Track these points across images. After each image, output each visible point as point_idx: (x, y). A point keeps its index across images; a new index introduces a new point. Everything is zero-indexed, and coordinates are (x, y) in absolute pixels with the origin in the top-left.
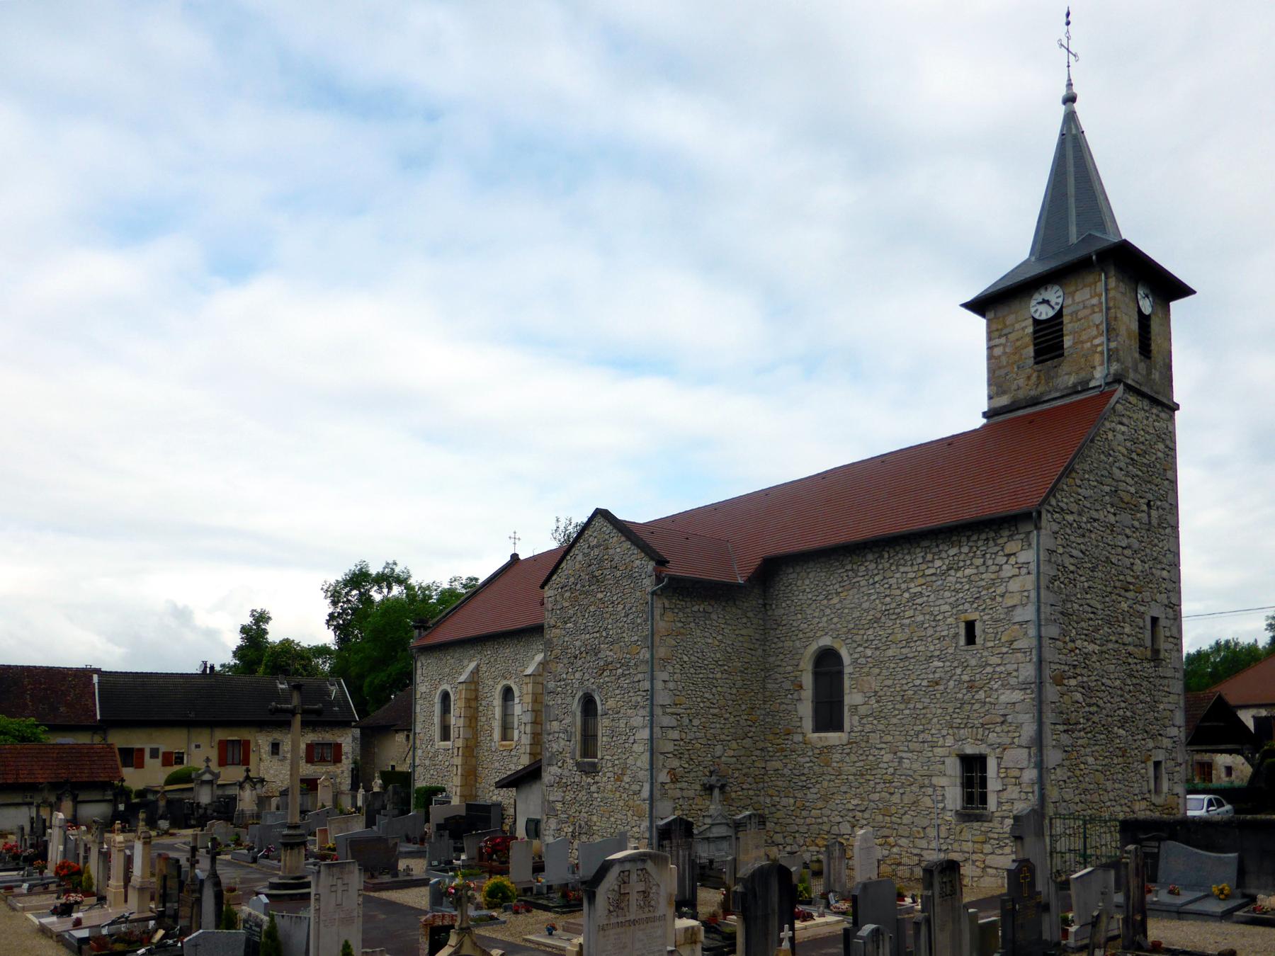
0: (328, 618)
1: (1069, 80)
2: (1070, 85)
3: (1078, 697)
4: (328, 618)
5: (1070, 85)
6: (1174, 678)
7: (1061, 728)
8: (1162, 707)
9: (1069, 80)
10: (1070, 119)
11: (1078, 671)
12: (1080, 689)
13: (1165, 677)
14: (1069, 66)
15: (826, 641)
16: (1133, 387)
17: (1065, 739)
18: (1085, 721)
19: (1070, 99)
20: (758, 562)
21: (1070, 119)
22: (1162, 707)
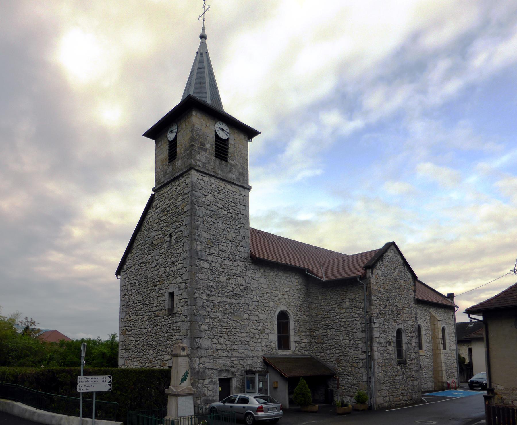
0: (58, 342)
1: (204, 27)
2: (203, 30)
3: (132, 338)
4: (58, 342)
5: (203, 30)
6: (184, 321)
7: (124, 351)
8: (175, 338)
9: (204, 27)
10: (203, 45)
11: (132, 328)
12: (133, 335)
13: (178, 322)
14: (204, 21)
15: (284, 308)
16: (160, 187)
17: (126, 355)
18: (134, 348)
19: (203, 37)
20: (52, 329)
21: (203, 45)
22: (175, 338)
